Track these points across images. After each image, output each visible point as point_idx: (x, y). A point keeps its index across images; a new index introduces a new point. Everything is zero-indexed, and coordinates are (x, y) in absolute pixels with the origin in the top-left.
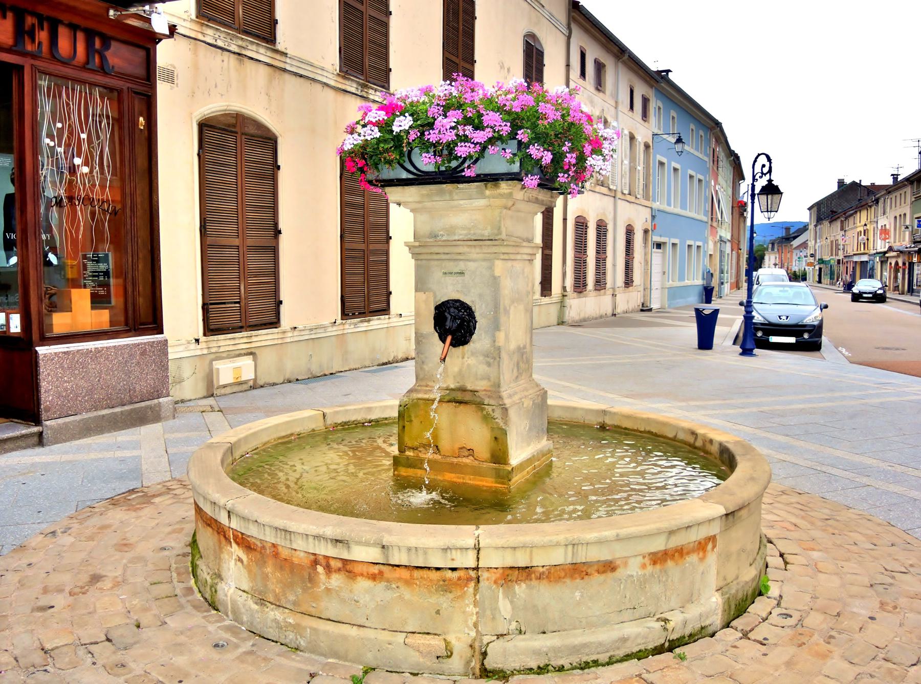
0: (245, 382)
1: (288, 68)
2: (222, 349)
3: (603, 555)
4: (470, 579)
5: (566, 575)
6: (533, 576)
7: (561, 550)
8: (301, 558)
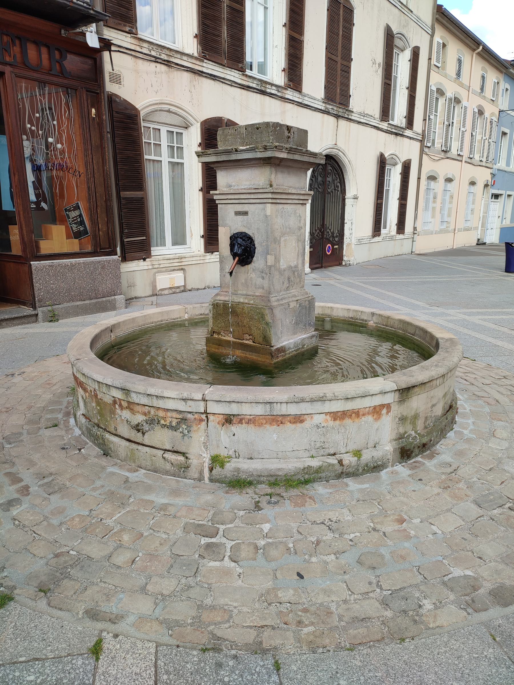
0: (178, 287)
1: (205, 70)
2: (162, 266)
3: (293, 410)
4: (201, 420)
5: (267, 422)
6: (244, 421)
7: (260, 406)
8: (108, 399)
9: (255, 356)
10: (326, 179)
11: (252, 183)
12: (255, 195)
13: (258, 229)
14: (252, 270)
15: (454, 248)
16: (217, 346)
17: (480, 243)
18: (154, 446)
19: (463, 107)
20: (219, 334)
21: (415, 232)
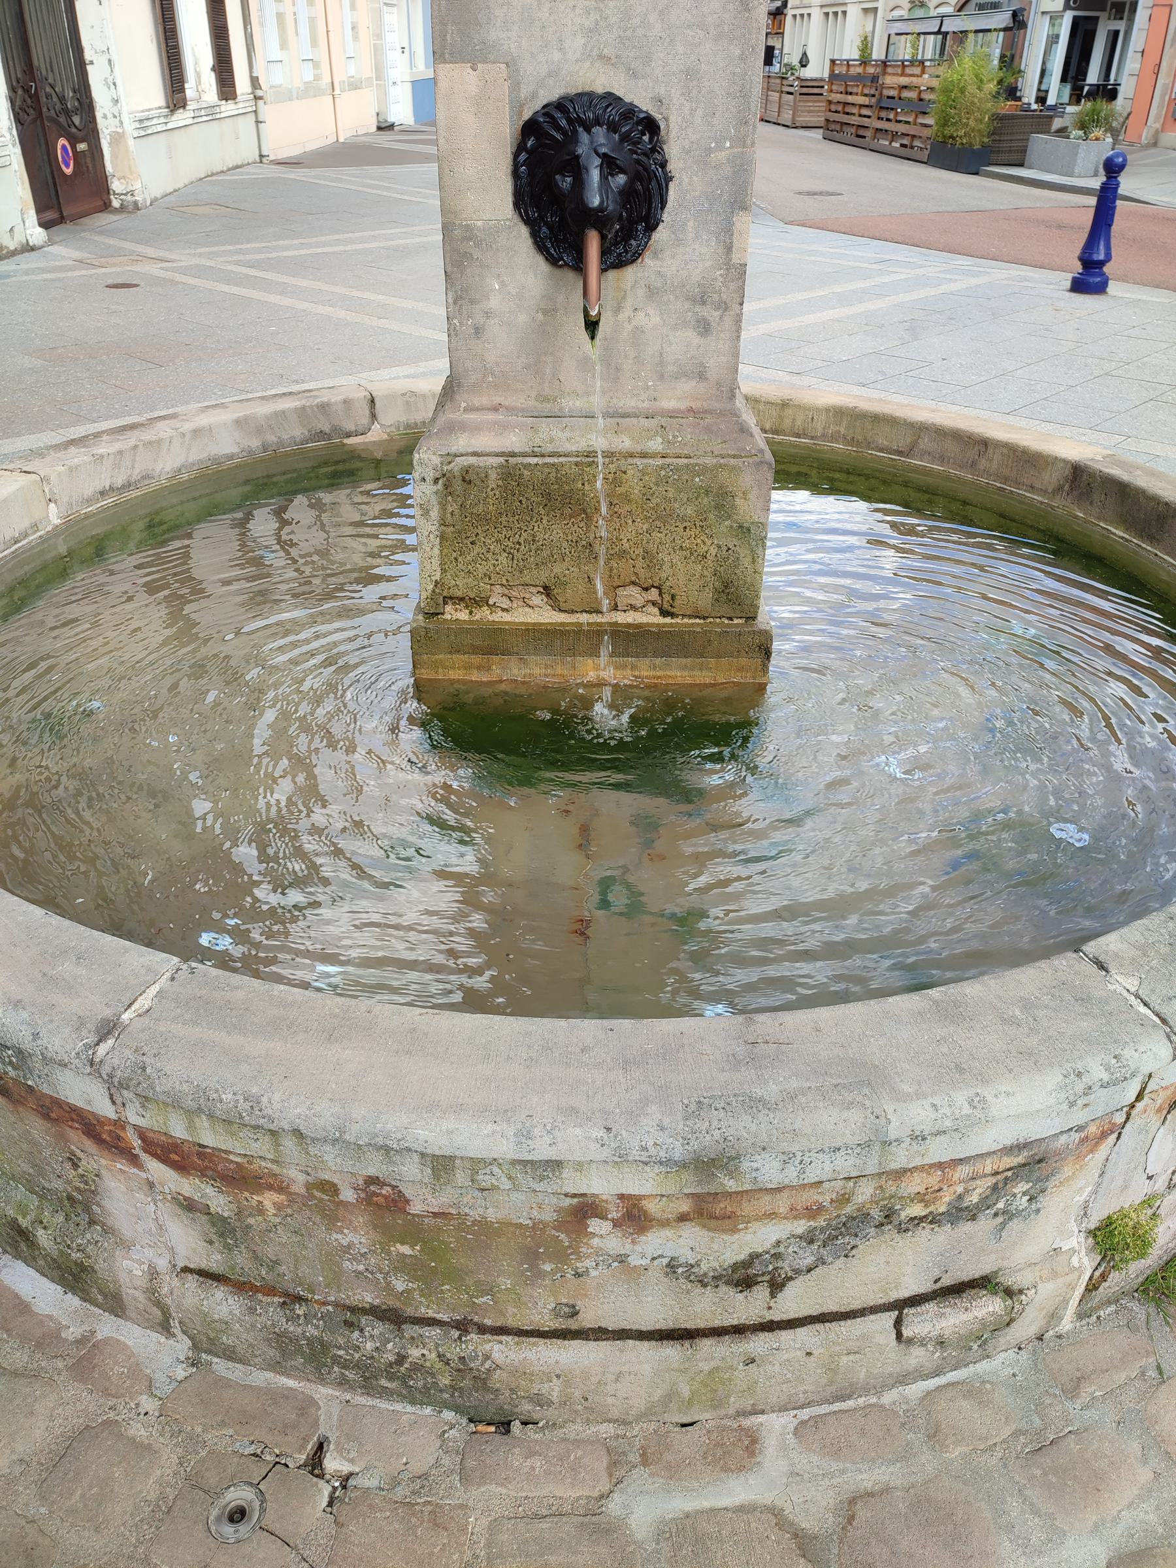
9: (684, 668)
13: (690, 74)
14: (641, 292)
15: (341, 140)
16: (476, 659)
17: (385, 127)
18: (834, 1308)
20: (476, 602)
21: (259, 93)
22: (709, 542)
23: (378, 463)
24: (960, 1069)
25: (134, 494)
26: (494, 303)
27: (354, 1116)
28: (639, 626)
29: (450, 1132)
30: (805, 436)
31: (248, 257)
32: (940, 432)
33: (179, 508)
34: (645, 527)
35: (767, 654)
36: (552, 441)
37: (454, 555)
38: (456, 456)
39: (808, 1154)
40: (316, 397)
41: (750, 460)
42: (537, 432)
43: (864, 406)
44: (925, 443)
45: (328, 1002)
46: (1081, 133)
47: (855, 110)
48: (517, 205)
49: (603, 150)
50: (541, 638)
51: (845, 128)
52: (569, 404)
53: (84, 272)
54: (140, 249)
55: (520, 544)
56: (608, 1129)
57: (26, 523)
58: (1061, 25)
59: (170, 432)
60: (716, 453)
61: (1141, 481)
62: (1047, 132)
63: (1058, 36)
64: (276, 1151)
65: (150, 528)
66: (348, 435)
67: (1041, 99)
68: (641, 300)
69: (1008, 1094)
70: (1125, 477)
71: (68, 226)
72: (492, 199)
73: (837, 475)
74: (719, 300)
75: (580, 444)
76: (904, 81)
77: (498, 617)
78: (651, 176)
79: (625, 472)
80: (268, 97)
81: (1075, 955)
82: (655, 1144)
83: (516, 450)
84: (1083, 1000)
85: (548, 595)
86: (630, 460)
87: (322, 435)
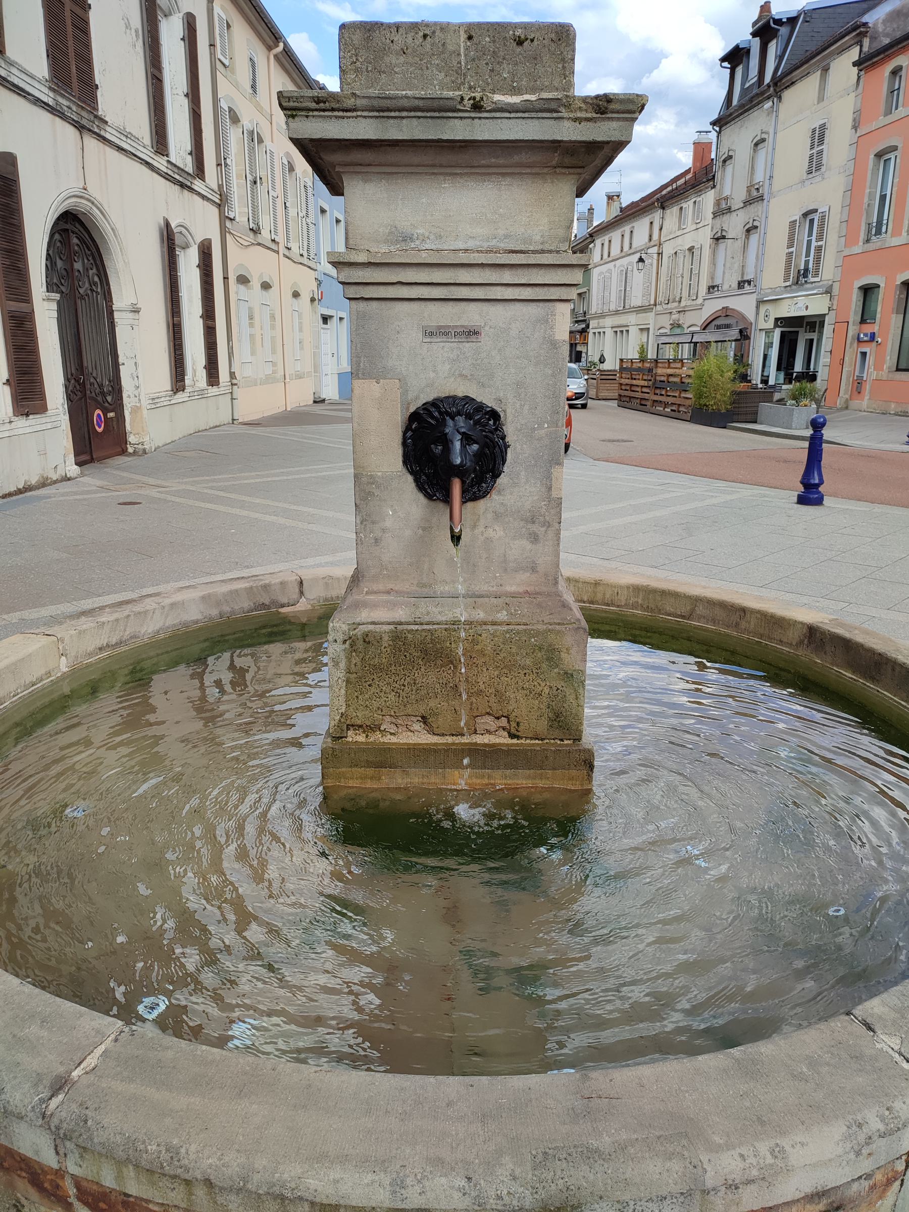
9: (529, 777)
10: (72, 266)
11: (501, 232)
12: (520, 271)
13: (519, 385)
14: (490, 516)
15: (289, 409)
16: (370, 771)
17: (318, 401)
19: (268, 152)
21: (234, 381)
22: (543, 684)
23: (303, 626)
24: (761, 1122)
25: (123, 649)
26: (388, 523)
27: (256, 1166)
28: (494, 745)
29: (336, 1182)
30: (613, 605)
31: (220, 484)
32: (711, 603)
33: (156, 659)
34: (496, 673)
35: (591, 767)
36: (428, 613)
37: (356, 694)
38: (359, 624)
39: (639, 1203)
40: (262, 580)
41: (570, 626)
42: (417, 607)
43: (654, 584)
44: (700, 610)
45: (241, 1061)
46: (794, 402)
47: (639, 389)
48: (405, 462)
49: (463, 430)
50: (420, 755)
51: (633, 400)
52: (440, 589)
53: (104, 495)
54: (145, 479)
55: (404, 686)
56: (469, 1179)
57: (43, 671)
58: (773, 336)
59: (155, 606)
60: (546, 621)
61: (859, 638)
62: (771, 402)
63: (772, 343)
64: (189, 1200)
65: (132, 674)
66: (283, 606)
67: (765, 381)
68: (489, 522)
69: (803, 1144)
70: (847, 635)
71: (96, 464)
72: (389, 459)
73: (638, 632)
74: (545, 520)
75: (448, 616)
76: (670, 371)
77: (389, 739)
78: (495, 444)
79: (480, 635)
80: (240, 384)
81: (847, 1018)
82: (509, 1193)
83: (403, 620)
84: (858, 1057)
85: (425, 723)
86: (484, 627)
87: (263, 606)
